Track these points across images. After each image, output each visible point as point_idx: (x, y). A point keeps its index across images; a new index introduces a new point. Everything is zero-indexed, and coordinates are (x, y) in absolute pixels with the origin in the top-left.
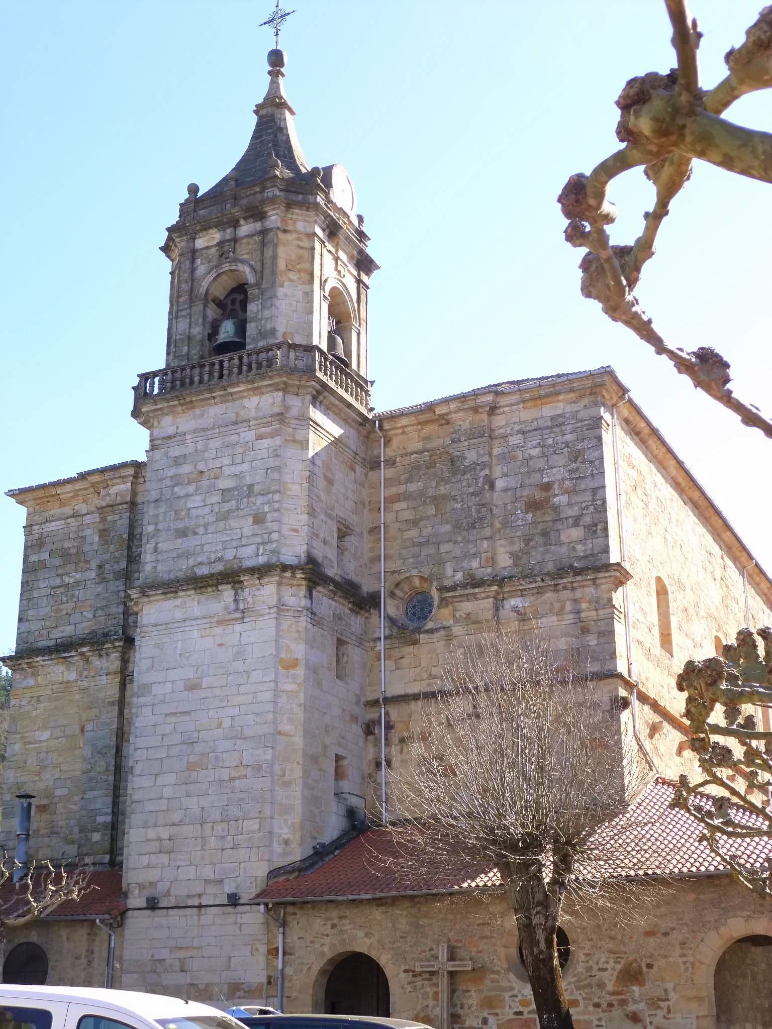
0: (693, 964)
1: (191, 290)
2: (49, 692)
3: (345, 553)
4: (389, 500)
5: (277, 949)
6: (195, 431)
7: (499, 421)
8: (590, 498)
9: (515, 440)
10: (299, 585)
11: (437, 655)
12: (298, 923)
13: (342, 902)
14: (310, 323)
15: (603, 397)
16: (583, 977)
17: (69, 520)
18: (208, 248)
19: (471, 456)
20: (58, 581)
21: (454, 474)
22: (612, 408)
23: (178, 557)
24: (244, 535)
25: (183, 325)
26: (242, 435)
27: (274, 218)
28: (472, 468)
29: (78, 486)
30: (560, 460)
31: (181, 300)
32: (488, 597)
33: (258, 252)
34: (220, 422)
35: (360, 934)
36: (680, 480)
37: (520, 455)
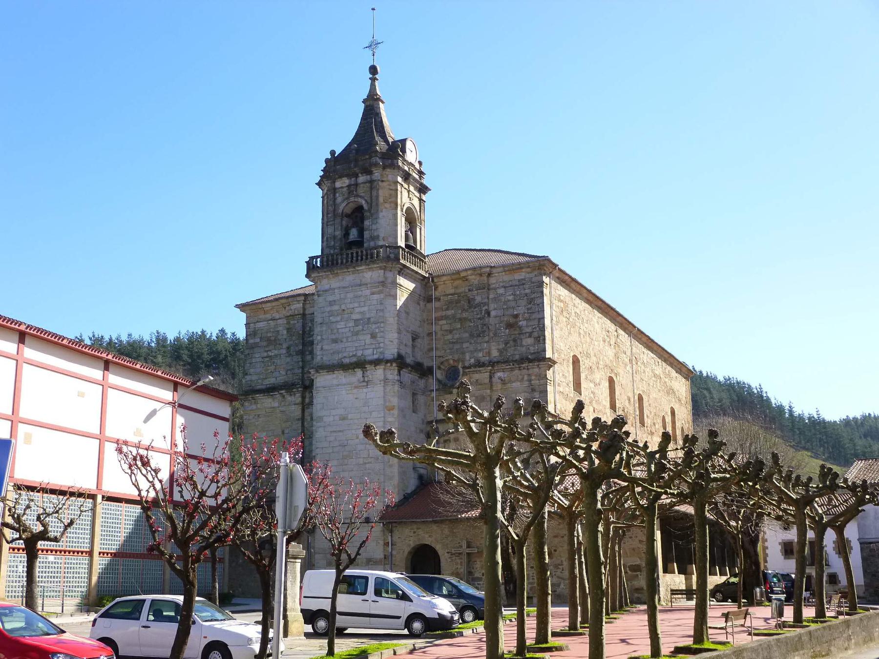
1: (334, 211)
2: (265, 413)
3: (416, 348)
4: (437, 319)
5: (388, 543)
7: (493, 280)
8: (537, 323)
9: (501, 291)
13: (418, 522)
14: (397, 231)
15: (545, 270)
18: (342, 187)
19: (478, 299)
20: (265, 354)
21: (470, 307)
22: (549, 275)
23: (334, 353)
25: (330, 230)
27: (377, 174)
28: (479, 305)
29: (274, 304)
30: (523, 302)
31: (330, 215)
32: (486, 372)
33: (369, 193)
35: (427, 536)
36: (590, 298)
37: (503, 299)
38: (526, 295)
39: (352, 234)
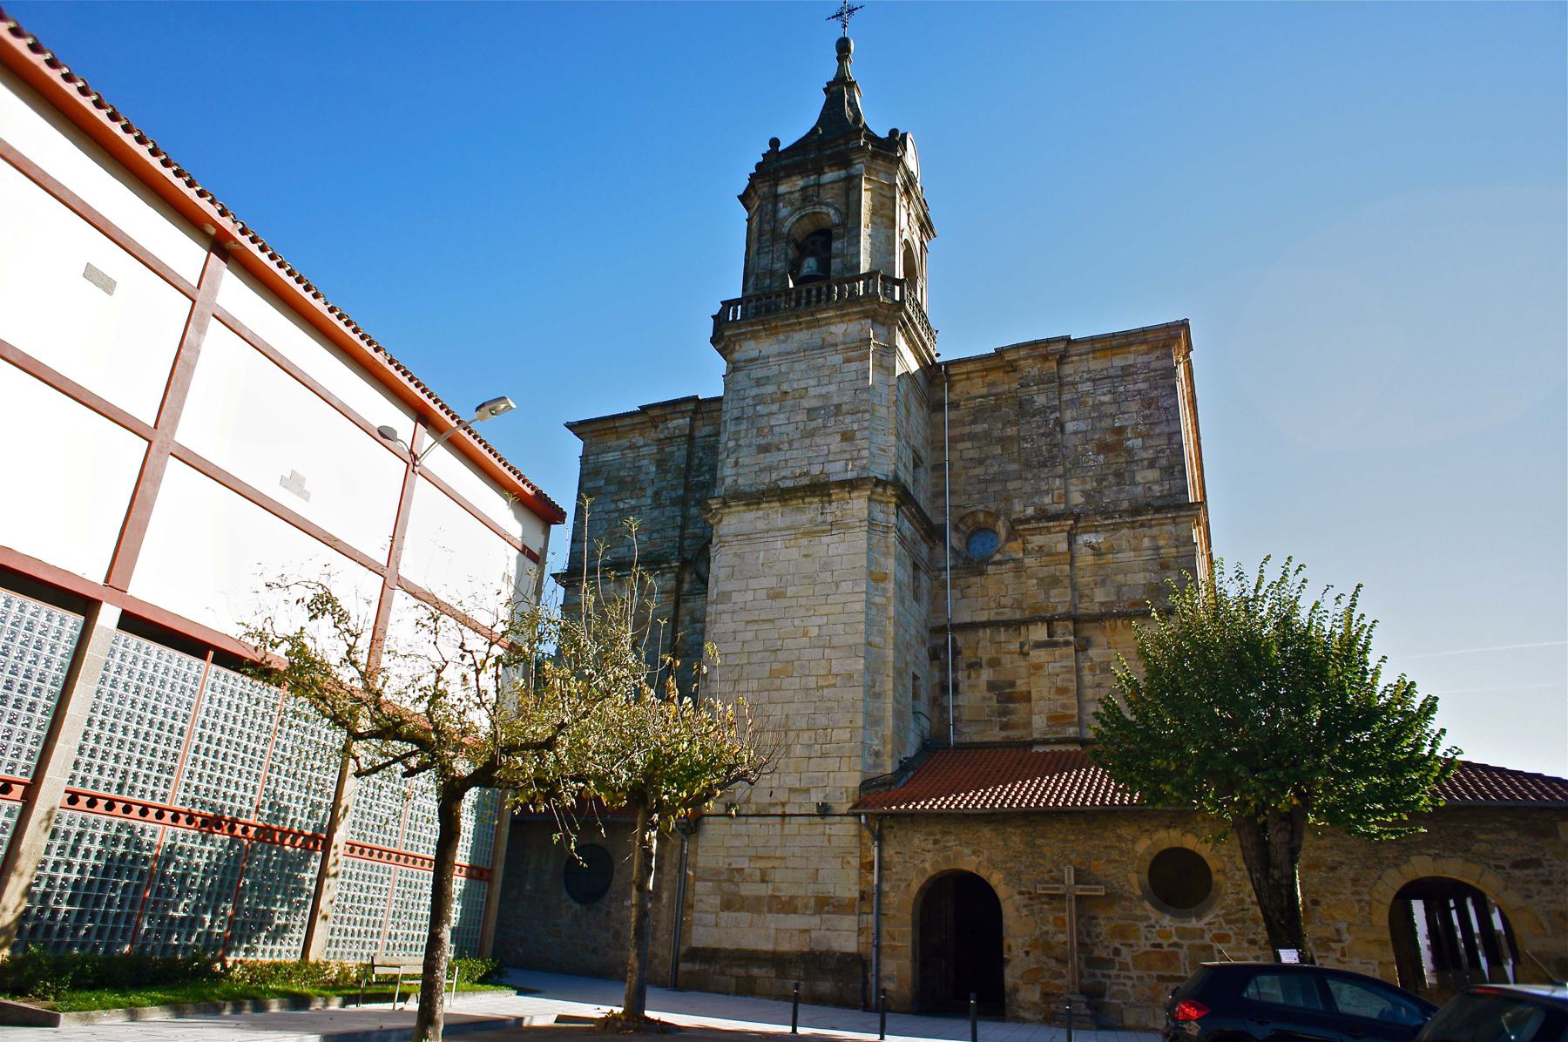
0: (1369, 903)
1: (774, 230)
6: (779, 354)
7: (1068, 369)
9: (1087, 387)
10: (888, 502)
11: (1006, 586)
12: (895, 837)
16: (1233, 910)
17: (626, 452)
18: (791, 193)
20: (613, 506)
21: (1023, 416)
23: (761, 471)
24: (832, 451)
26: (829, 358)
28: (1042, 411)
30: (1133, 406)
31: (764, 238)
34: (805, 346)
35: (967, 851)
38: (1139, 392)
39: (806, 265)
